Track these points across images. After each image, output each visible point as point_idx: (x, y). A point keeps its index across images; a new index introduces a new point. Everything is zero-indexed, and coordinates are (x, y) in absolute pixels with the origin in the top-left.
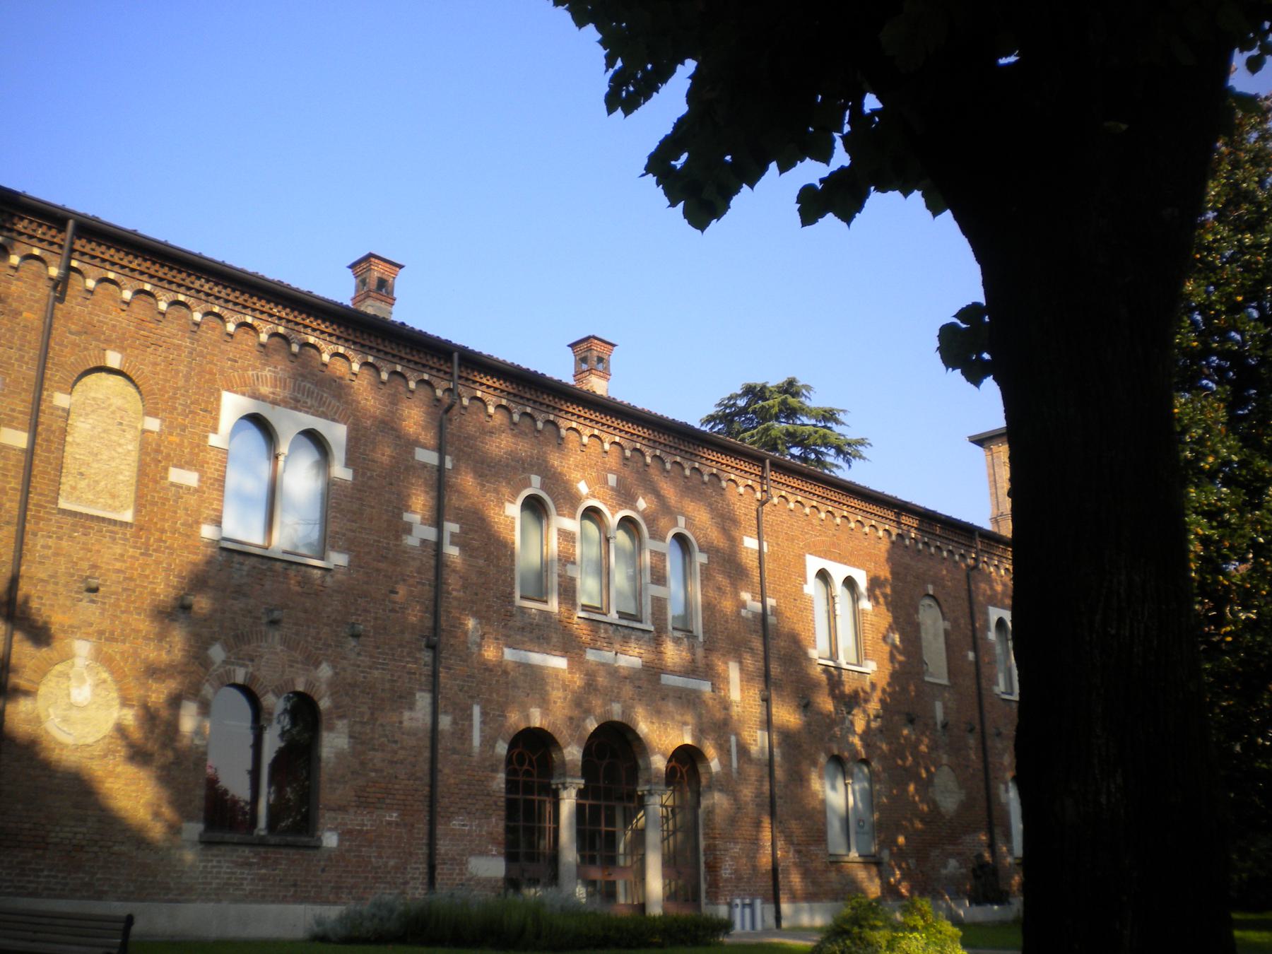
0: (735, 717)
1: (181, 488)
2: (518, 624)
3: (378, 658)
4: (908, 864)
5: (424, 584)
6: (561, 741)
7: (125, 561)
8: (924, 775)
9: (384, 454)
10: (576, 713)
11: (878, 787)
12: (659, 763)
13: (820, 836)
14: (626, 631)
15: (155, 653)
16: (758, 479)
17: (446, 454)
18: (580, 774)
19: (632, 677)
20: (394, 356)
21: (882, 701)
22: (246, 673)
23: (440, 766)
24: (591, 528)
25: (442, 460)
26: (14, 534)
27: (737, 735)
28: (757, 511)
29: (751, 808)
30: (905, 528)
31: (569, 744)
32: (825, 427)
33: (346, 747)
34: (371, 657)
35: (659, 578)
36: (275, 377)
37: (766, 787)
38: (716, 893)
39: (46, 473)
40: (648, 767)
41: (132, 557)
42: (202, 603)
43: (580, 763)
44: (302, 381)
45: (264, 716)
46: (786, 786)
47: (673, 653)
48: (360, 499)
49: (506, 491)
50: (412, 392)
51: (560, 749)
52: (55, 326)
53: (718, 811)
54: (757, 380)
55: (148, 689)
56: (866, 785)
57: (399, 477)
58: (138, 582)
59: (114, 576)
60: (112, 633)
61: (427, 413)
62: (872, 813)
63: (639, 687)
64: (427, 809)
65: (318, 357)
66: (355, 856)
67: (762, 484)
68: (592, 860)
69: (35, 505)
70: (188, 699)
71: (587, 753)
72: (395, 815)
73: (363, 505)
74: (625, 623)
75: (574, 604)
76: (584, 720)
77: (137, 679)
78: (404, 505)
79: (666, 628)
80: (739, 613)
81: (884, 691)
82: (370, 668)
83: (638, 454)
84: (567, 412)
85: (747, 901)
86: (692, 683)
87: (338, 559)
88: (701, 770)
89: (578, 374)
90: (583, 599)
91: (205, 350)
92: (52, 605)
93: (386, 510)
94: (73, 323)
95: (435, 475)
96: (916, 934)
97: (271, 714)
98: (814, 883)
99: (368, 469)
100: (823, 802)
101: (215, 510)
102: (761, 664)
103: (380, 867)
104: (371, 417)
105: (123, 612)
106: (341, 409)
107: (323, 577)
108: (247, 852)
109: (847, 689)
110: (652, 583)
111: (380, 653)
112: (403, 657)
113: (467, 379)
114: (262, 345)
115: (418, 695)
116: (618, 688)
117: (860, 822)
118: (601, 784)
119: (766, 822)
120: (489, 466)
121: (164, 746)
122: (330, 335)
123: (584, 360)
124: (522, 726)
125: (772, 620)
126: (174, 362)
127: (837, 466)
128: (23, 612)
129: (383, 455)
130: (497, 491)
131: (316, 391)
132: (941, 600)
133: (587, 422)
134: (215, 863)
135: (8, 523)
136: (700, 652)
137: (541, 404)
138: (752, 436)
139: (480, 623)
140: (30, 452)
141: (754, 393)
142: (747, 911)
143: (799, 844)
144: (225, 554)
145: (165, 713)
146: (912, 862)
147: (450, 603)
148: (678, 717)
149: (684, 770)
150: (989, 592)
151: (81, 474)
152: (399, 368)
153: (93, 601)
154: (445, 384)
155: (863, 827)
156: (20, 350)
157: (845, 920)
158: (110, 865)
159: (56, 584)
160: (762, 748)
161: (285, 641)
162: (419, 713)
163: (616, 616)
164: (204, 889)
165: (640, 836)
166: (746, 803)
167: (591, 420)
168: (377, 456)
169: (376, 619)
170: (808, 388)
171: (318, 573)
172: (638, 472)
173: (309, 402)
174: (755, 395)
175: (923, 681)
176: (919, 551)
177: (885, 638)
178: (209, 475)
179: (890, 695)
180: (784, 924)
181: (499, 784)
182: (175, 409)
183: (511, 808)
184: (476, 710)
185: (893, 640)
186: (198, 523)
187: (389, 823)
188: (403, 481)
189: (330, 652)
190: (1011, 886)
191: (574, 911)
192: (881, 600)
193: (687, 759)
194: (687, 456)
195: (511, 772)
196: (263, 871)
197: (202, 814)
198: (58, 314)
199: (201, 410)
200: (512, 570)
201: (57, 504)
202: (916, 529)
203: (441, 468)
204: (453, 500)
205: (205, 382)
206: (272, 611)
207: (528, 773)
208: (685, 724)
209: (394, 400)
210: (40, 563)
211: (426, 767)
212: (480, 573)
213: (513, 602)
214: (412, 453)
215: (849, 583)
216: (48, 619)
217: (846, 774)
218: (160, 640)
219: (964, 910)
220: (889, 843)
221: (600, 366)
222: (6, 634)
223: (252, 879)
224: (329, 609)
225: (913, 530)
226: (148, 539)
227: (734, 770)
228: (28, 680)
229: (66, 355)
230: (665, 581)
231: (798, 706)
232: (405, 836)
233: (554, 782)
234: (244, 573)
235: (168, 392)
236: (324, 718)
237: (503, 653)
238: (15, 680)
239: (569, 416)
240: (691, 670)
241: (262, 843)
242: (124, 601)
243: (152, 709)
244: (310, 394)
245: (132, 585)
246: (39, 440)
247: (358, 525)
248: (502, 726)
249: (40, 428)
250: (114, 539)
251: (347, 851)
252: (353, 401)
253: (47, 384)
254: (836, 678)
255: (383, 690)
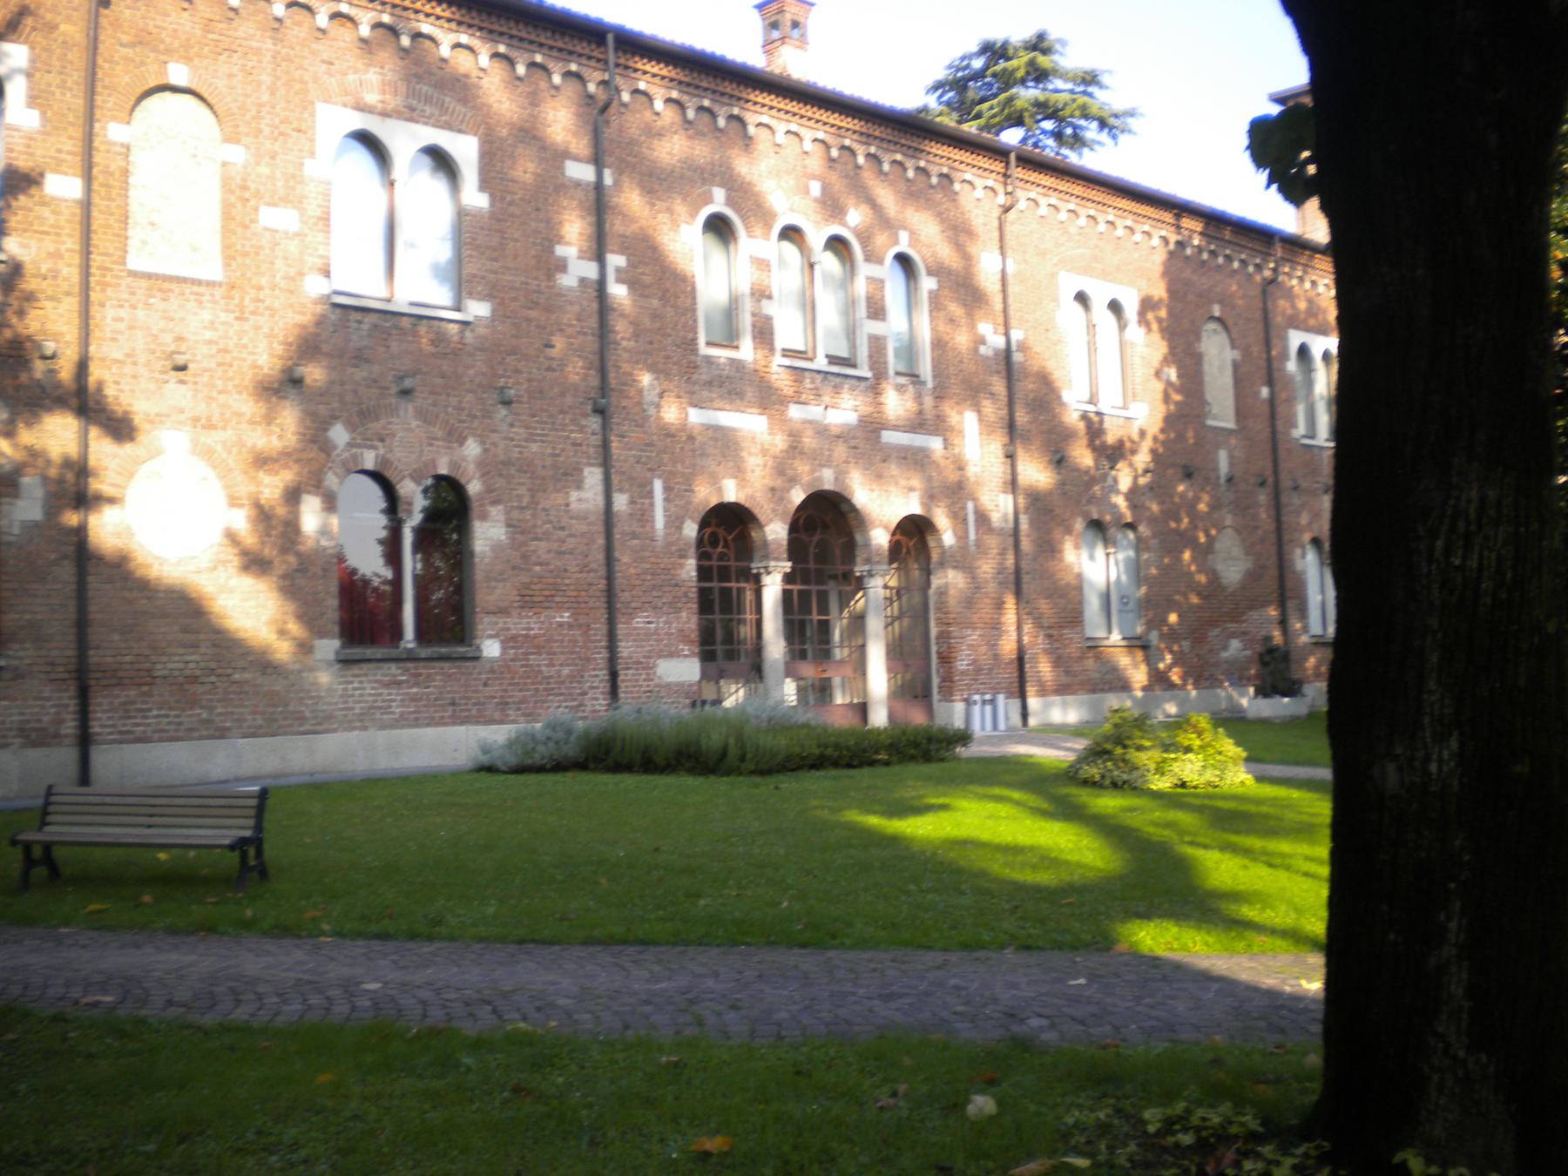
0: (972, 479)
1: (277, 231)
2: (704, 377)
3: (535, 428)
4: (1180, 646)
5: (585, 334)
6: (762, 517)
7: (216, 329)
8: (1202, 539)
9: (526, 169)
10: (779, 483)
11: (1146, 556)
12: (880, 538)
13: (1073, 616)
14: (838, 380)
15: (264, 440)
16: (1000, 178)
17: (604, 167)
18: (785, 556)
19: (844, 436)
20: (531, 42)
21: (1153, 451)
22: (377, 457)
23: (617, 554)
24: (789, 248)
25: (599, 175)
26: (76, 307)
27: (975, 500)
28: (1000, 218)
29: (991, 587)
30: (1186, 233)
31: (771, 520)
32: (1084, 93)
33: (503, 537)
34: (527, 427)
35: (877, 311)
36: (383, 81)
37: (1010, 561)
38: (950, 687)
39: (109, 226)
40: (867, 544)
41: (225, 323)
42: (314, 374)
43: (785, 543)
44: (418, 83)
45: (401, 507)
46: (1035, 559)
47: (895, 404)
48: (500, 231)
49: (680, 209)
50: (557, 88)
51: (760, 526)
52: (102, 38)
53: (952, 592)
54: (997, 35)
55: (259, 483)
56: (1131, 553)
57: (546, 199)
58: (235, 354)
59: (205, 350)
60: (209, 419)
61: (577, 115)
62: (1139, 587)
63: (855, 448)
64: (605, 605)
65: (435, 50)
66: (523, 666)
67: (1005, 184)
68: (803, 655)
69: (99, 268)
70: (309, 492)
71: (794, 528)
72: (567, 614)
73: (503, 238)
74: (835, 369)
75: (772, 349)
76: (788, 491)
77: (245, 473)
78: (556, 236)
79: (886, 373)
80: (976, 350)
81: (1155, 439)
82: (527, 441)
83: (846, 153)
84: (755, 103)
85: (988, 697)
86: (918, 440)
87: (478, 309)
88: (932, 543)
89: (769, 46)
90: (781, 341)
91: (292, 52)
92: (133, 391)
93: (534, 244)
94: (124, 33)
95: (592, 195)
96: (1190, 756)
97: (410, 504)
98: (1067, 673)
99: (509, 193)
100: (1079, 576)
101: (321, 257)
102: (1004, 412)
103: (551, 677)
104: (507, 124)
105: (220, 392)
106: (469, 115)
107: (462, 332)
108: (393, 668)
109: (1110, 439)
110: (869, 317)
111: (537, 422)
112: (565, 425)
113: (627, 67)
114: (363, 40)
115: (587, 471)
116: (829, 450)
117: (1124, 599)
118: (812, 566)
119: (1010, 603)
120: (659, 179)
121: (284, 550)
122: (449, 20)
123: (774, 25)
124: (714, 501)
125: (1017, 357)
126: (254, 71)
127: (1099, 143)
128: (98, 402)
129: (525, 172)
130: (670, 211)
131: (435, 95)
132: (1230, 322)
133: (782, 115)
134: (356, 685)
135: (68, 294)
136: (929, 401)
137: (723, 94)
138: (991, 108)
139: (657, 379)
140: (86, 205)
141: (994, 51)
142: (988, 708)
143: (1049, 628)
144: (338, 311)
145: (281, 511)
146: (1186, 644)
147: (619, 355)
148: (903, 482)
149: (911, 544)
150: (1289, 312)
151: (152, 224)
152: (538, 58)
153: (182, 382)
154: (598, 76)
155: (1126, 604)
156: (61, 73)
157: (1107, 738)
158: (232, 696)
159: (135, 364)
160: (1005, 515)
161: (421, 414)
162: (589, 492)
163: (825, 361)
164: (345, 716)
165: (859, 621)
166: (986, 581)
167: (787, 112)
168: (518, 173)
169: (529, 380)
170: (1063, 43)
171: (454, 328)
172: (847, 177)
173: (428, 110)
174: (994, 53)
175: (1204, 426)
176: (1204, 262)
177: (1158, 374)
178: (310, 213)
179: (1164, 443)
180: (1032, 722)
181: (688, 572)
182: (260, 131)
183: (705, 603)
184: (658, 485)
185: (1168, 376)
186: (301, 274)
187: (561, 625)
188: (552, 205)
189: (476, 424)
190: (1305, 669)
191: (780, 724)
192: (1155, 326)
193: (915, 531)
194: (910, 152)
195: (702, 556)
196: (415, 690)
197: (336, 629)
198: (104, 22)
199: (294, 130)
200: (694, 311)
201: (124, 264)
202: (1201, 233)
203: (599, 186)
204: (616, 226)
205: (296, 93)
206: (402, 378)
207: (722, 557)
208: (911, 489)
209: (534, 100)
210: (114, 340)
211: (600, 556)
212: (655, 316)
213: (697, 350)
214: (561, 169)
215: (1115, 307)
216: (128, 409)
217: (1107, 542)
218: (269, 424)
219: (1246, 700)
220: (1156, 622)
221: (796, 34)
222: (79, 431)
223: (402, 700)
224: (471, 372)
225: (1195, 236)
226: (242, 299)
227: (971, 543)
228: (114, 485)
229: (119, 76)
230: (884, 315)
231: (1050, 462)
232: (579, 638)
233: (755, 566)
234: (365, 333)
235: (249, 110)
236: (475, 506)
237: (687, 414)
238: (95, 485)
239: (757, 108)
240: (918, 424)
241: (410, 658)
242: (220, 378)
243: (267, 508)
244: (428, 100)
245: (228, 358)
246: (95, 186)
247: (500, 264)
248: (689, 503)
249: (95, 171)
250: (200, 302)
251: (513, 660)
252: (484, 104)
253: (98, 114)
254: (1097, 426)
255: (544, 467)
